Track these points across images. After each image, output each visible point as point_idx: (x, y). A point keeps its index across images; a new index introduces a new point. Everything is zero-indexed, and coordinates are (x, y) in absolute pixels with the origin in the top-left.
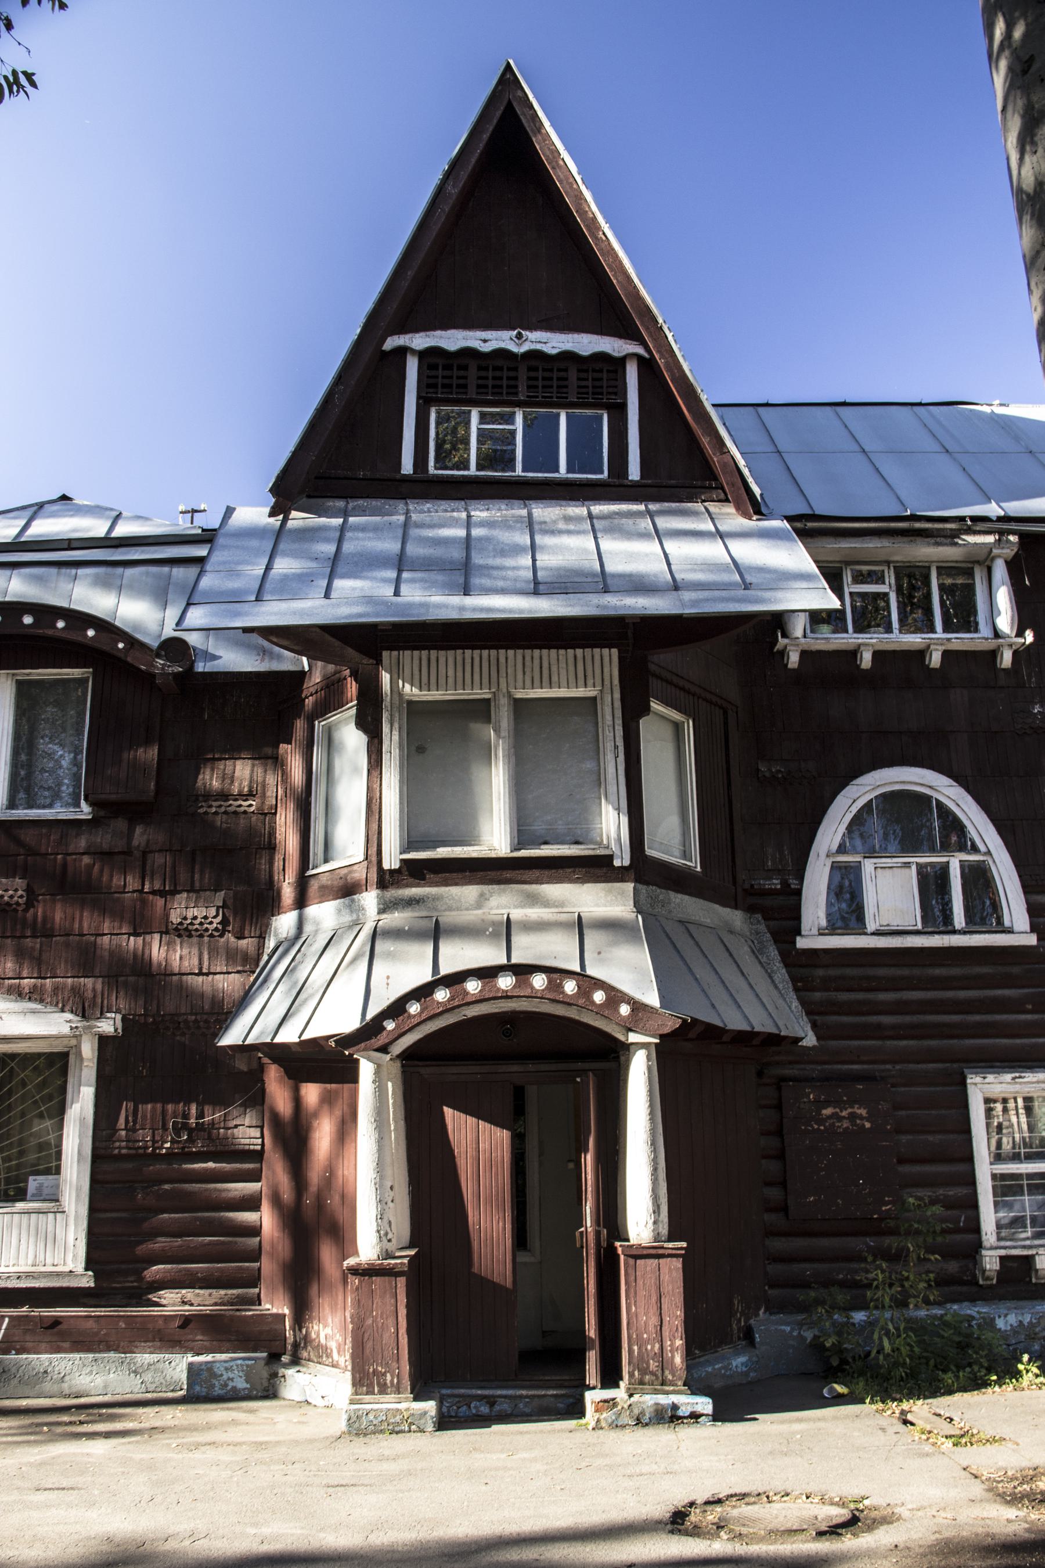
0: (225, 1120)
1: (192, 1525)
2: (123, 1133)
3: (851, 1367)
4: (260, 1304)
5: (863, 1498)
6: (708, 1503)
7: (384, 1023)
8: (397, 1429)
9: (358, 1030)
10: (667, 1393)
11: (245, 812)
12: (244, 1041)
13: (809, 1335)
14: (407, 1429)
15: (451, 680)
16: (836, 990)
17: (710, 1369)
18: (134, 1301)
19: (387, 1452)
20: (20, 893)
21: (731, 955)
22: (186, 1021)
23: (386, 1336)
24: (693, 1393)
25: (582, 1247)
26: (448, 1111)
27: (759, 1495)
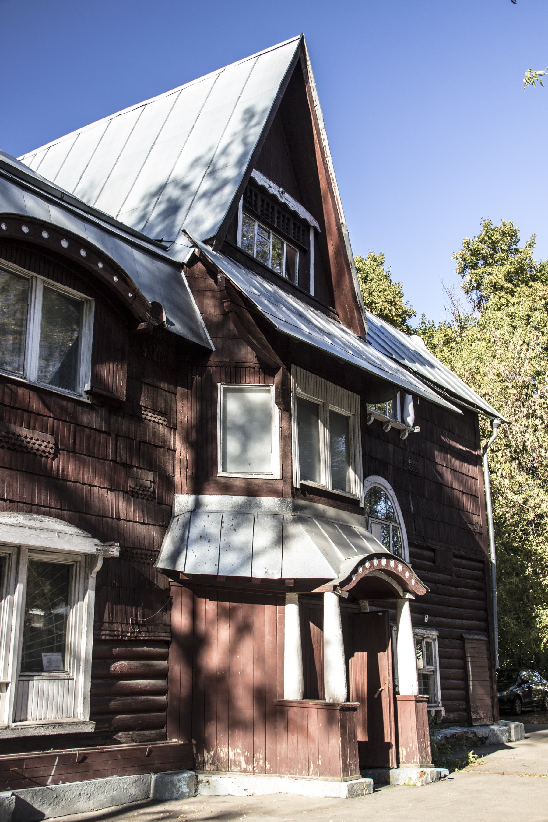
4: (167, 740)
18: (108, 741)
20: (51, 445)
22: (137, 553)
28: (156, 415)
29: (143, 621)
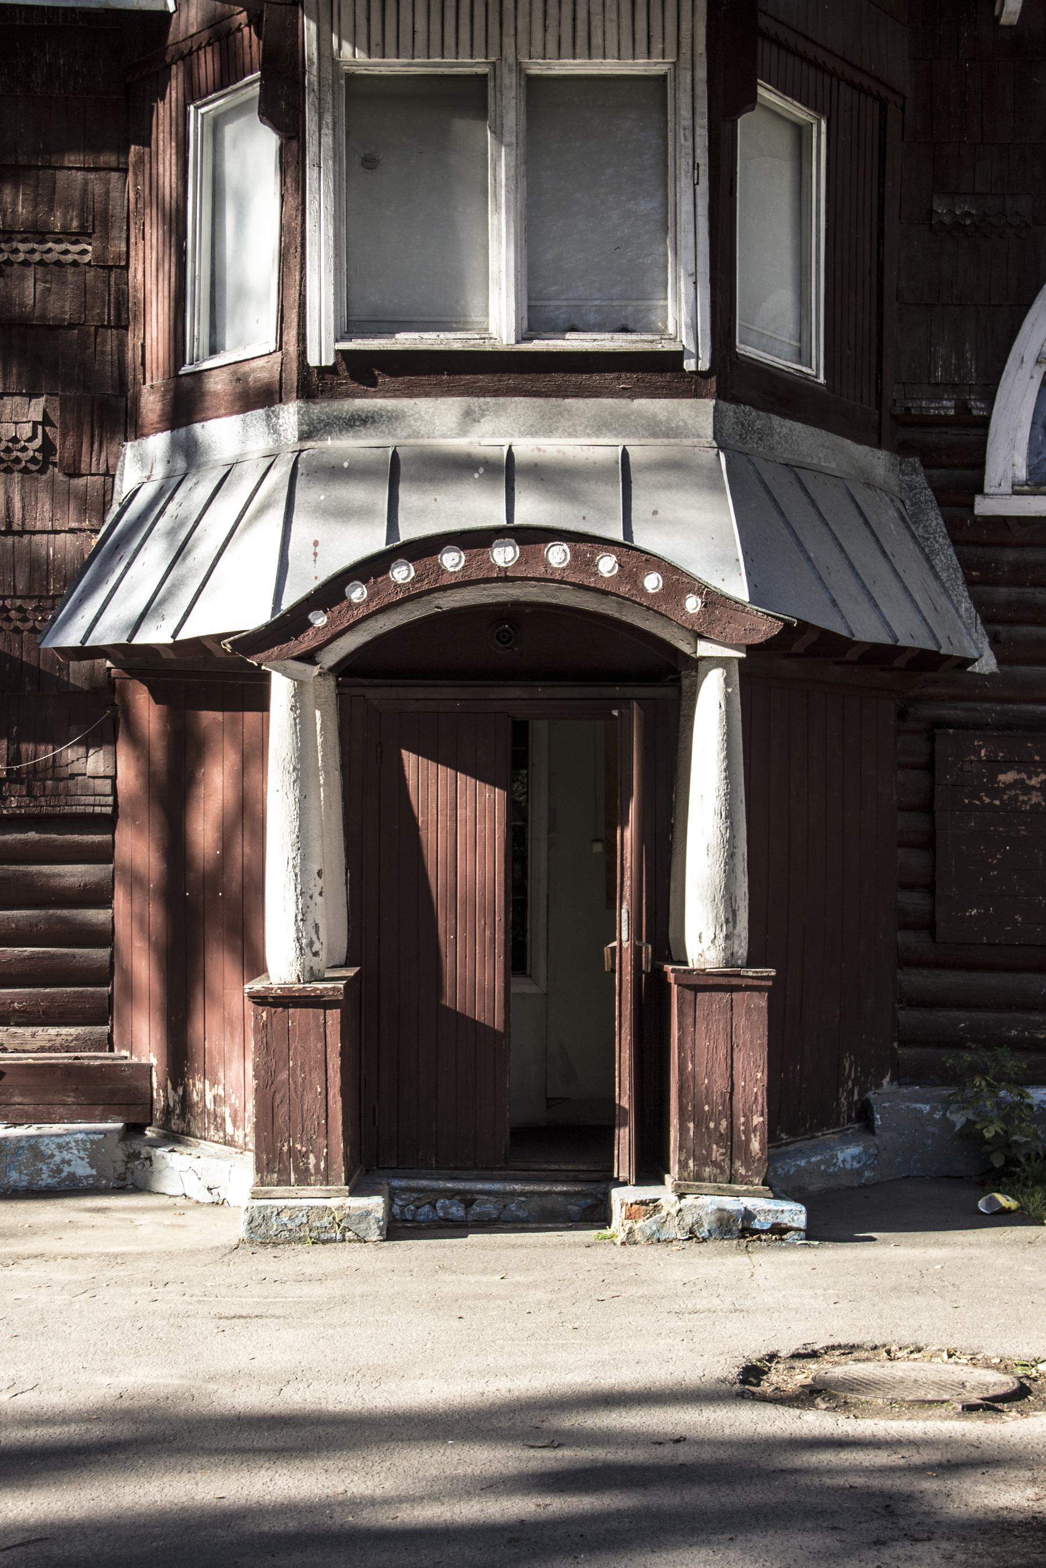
1: (12, 1372)
3: (1024, 1170)
4: (112, 1050)
5: (1037, 1361)
6: (796, 1356)
7: (310, 616)
8: (324, 1236)
9: (268, 626)
10: (737, 1194)
11: (75, 264)
12: (83, 642)
13: (958, 1119)
14: (339, 1236)
15: (421, 39)
16: (1034, 584)
17: (803, 1163)
19: (308, 1271)
21: (866, 522)
23: (309, 1097)
24: (777, 1197)
25: (613, 971)
26: (409, 758)
27: (875, 1348)
28: (30, 246)
29: (8, 771)
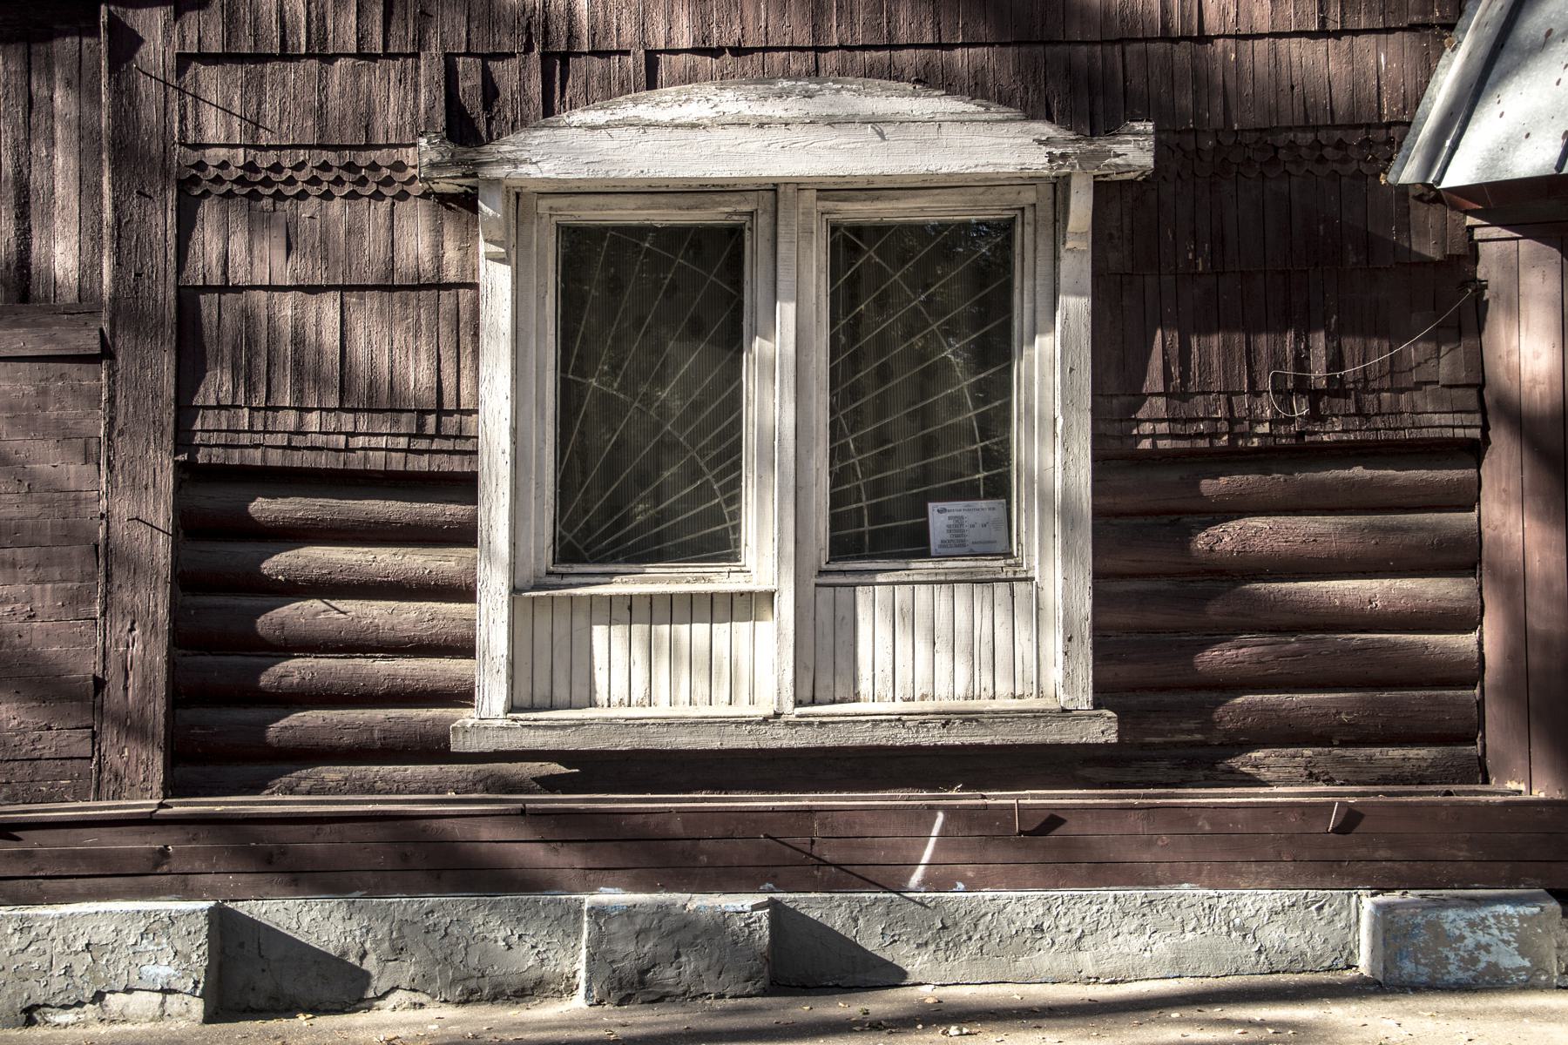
0: (1392, 372)
2: (1161, 402)
4: (1486, 781)
18: (1200, 774)
22: (1292, 145)
29: (1329, 379)
